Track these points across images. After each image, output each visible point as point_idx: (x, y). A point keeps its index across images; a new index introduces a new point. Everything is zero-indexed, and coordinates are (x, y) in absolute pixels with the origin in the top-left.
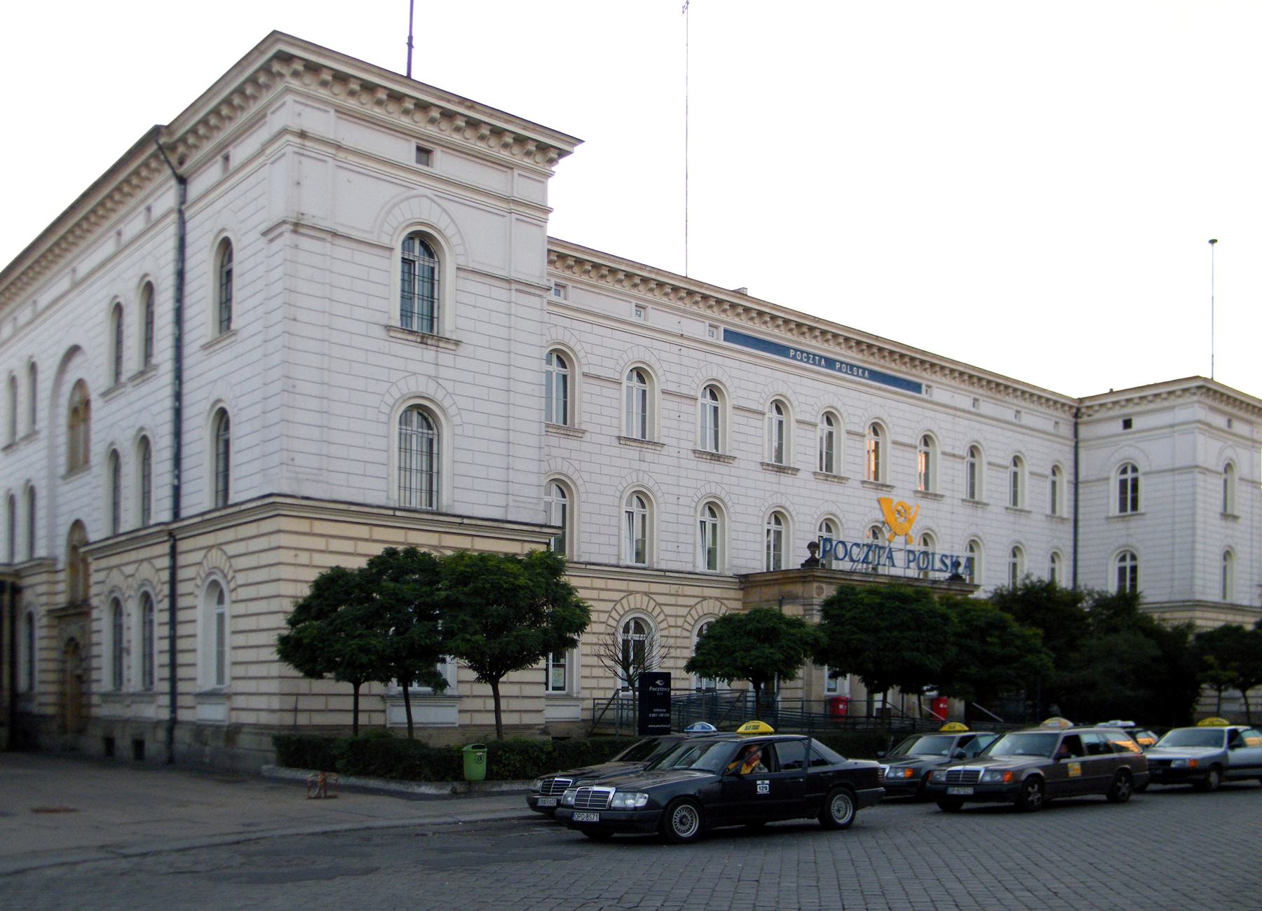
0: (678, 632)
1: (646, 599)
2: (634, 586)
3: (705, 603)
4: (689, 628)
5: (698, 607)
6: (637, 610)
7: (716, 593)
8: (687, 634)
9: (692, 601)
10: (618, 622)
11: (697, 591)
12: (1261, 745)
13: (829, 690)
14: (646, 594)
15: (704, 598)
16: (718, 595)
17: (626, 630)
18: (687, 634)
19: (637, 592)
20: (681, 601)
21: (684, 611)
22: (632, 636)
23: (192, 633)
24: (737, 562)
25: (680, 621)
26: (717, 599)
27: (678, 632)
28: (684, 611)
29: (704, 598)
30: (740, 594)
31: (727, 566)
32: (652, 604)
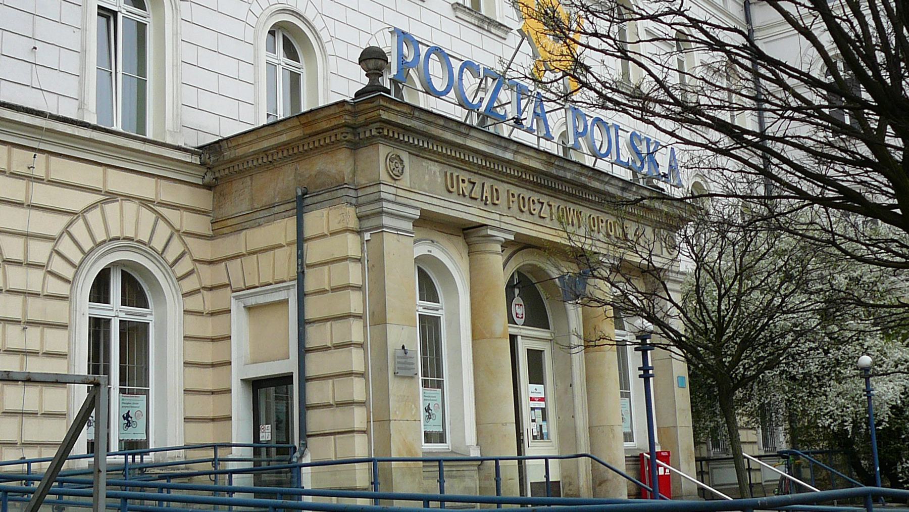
0: (34, 280)
1: (148, 217)
2: (118, 182)
3: (112, 209)
4: (68, 272)
5: (94, 217)
6: (131, 243)
7: (145, 188)
8: (62, 289)
9: (77, 201)
10: (77, 267)
11: (90, 176)
12: (6, 430)
13: (429, 437)
14: (145, 202)
15: (112, 197)
16: (149, 194)
17: (100, 292)
18: (62, 289)
19: (129, 198)
20: (42, 194)
21: (53, 225)
22: (115, 310)
23: (192, 426)
24: (192, 118)
25: (39, 252)
26: (145, 202)
27: (34, 280)
28: (53, 225)
29: (112, 197)
30: (203, 200)
31: (169, 125)
32: (163, 231)
